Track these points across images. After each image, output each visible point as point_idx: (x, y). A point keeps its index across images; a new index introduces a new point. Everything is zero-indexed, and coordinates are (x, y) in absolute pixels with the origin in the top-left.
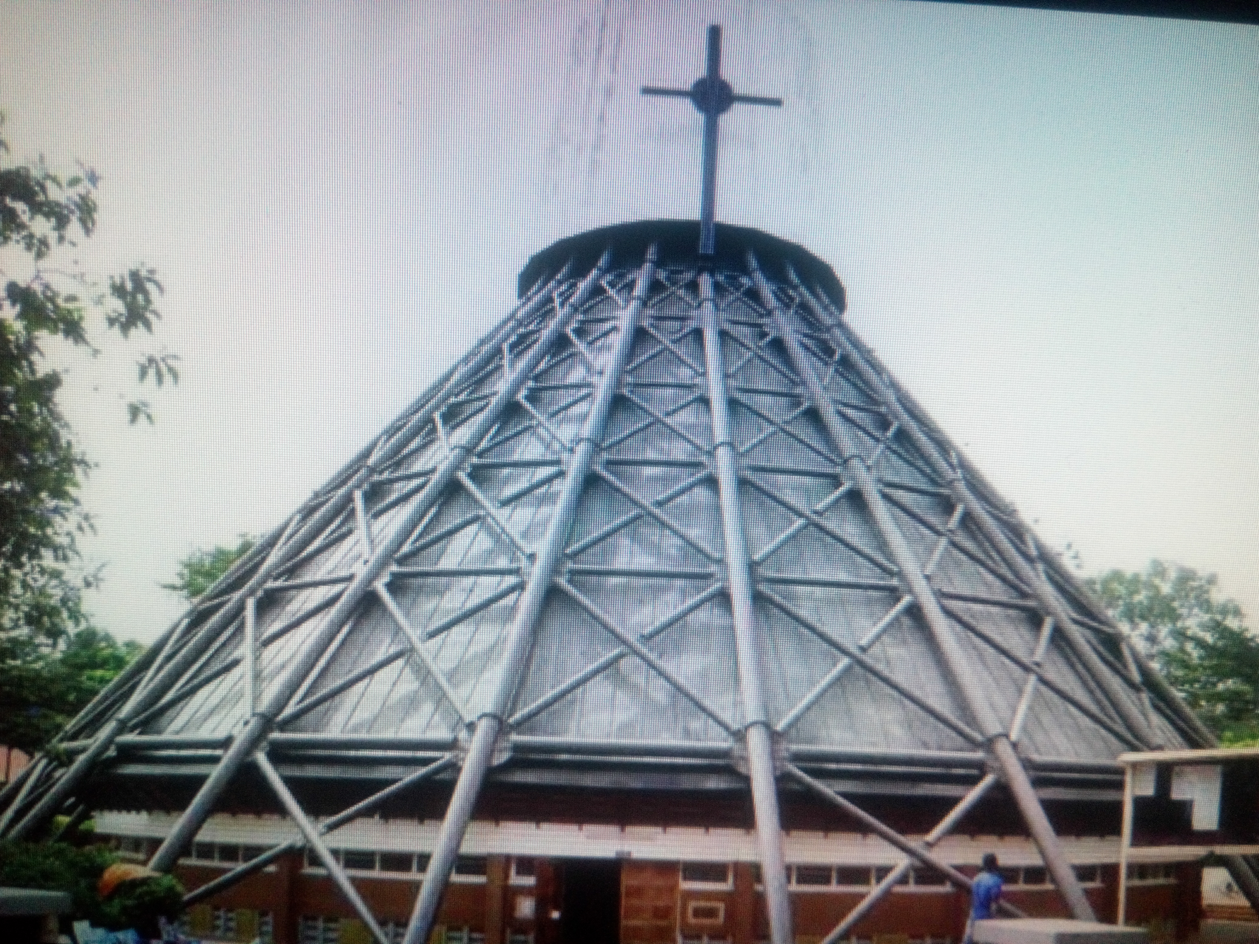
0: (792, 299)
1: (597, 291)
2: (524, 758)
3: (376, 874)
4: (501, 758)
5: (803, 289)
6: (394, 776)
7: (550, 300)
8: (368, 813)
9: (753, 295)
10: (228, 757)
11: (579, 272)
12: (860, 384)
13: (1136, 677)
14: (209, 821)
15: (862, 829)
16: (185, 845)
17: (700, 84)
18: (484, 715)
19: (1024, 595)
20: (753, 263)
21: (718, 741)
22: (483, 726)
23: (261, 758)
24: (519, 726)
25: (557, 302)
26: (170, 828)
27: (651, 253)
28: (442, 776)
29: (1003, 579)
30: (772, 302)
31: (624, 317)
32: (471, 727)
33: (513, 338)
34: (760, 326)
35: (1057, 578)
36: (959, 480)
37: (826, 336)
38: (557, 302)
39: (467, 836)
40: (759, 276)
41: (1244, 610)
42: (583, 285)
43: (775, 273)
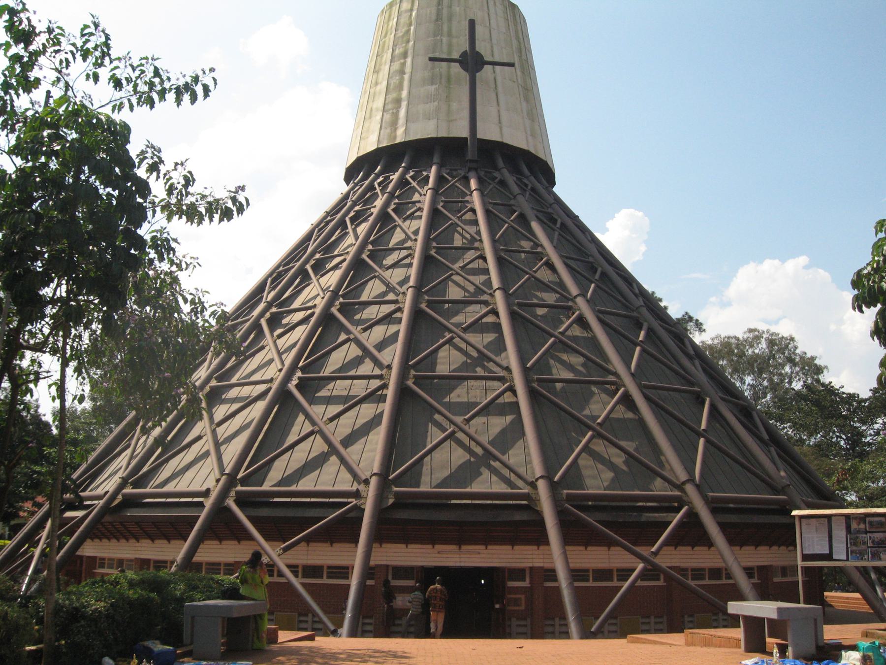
0: (526, 185)
1: (403, 183)
2: (403, 502)
3: (325, 581)
5: (532, 178)
6: (321, 515)
7: (371, 187)
8: (308, 539)
9: (503, 183)
10: (208, 503)
11: (390, 168)
12: (574, 242)
13: (766, 436)
14: (201, 546)
15: (610, 543)
16: (188, 563)
17: (464, 54)
18: (375, 474)
19: (692, 384)
20: (500, 163)
21: (526, 490)
22: (374, 481)
23: (231, 503)
24: (397, 481)
25: (378, 190)
26: (177, 552)
27: (436, 159)
28: (352, 515)
29: (677, 373)
30: (515, 189)
31: (424, 198)
32: (367, 482)
33: (352, 214)
34: (510, 206)
35: (601, 250)
36: (642, 306)
37: (550, 210)
38: (378, 190)
39: (373, 554)
40: (505, 172)
41: (796, 339)
42: (395, 177)
43: (516, 171)
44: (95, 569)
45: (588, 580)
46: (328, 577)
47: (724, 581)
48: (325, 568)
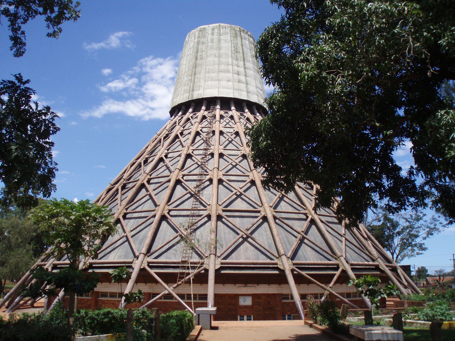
4: (218, 267)
42: (185, 117)
44: (99, 298)
45: (288, 299)
46: (199, 299)
47: (290, 301)
48: (117, 296)
